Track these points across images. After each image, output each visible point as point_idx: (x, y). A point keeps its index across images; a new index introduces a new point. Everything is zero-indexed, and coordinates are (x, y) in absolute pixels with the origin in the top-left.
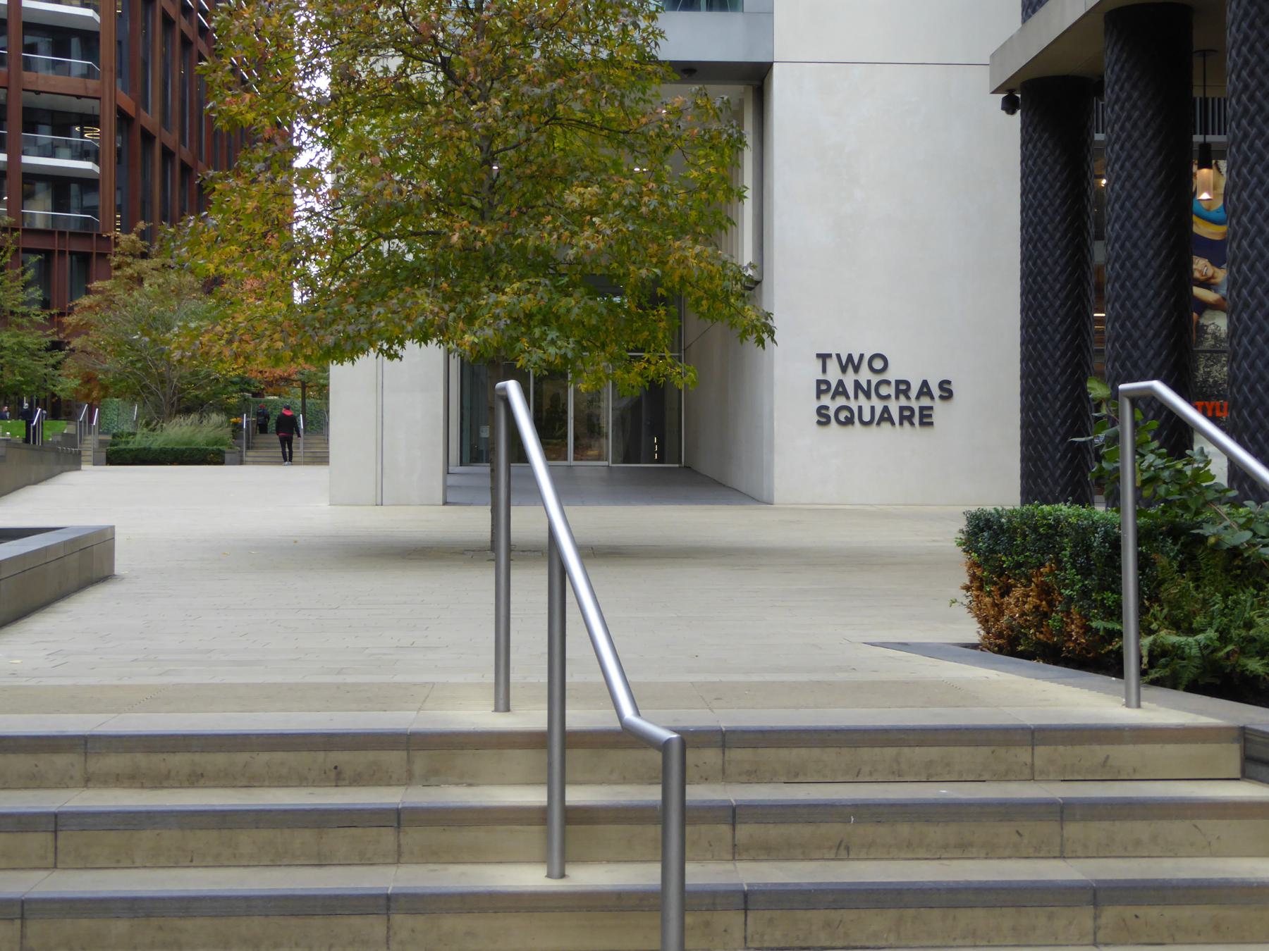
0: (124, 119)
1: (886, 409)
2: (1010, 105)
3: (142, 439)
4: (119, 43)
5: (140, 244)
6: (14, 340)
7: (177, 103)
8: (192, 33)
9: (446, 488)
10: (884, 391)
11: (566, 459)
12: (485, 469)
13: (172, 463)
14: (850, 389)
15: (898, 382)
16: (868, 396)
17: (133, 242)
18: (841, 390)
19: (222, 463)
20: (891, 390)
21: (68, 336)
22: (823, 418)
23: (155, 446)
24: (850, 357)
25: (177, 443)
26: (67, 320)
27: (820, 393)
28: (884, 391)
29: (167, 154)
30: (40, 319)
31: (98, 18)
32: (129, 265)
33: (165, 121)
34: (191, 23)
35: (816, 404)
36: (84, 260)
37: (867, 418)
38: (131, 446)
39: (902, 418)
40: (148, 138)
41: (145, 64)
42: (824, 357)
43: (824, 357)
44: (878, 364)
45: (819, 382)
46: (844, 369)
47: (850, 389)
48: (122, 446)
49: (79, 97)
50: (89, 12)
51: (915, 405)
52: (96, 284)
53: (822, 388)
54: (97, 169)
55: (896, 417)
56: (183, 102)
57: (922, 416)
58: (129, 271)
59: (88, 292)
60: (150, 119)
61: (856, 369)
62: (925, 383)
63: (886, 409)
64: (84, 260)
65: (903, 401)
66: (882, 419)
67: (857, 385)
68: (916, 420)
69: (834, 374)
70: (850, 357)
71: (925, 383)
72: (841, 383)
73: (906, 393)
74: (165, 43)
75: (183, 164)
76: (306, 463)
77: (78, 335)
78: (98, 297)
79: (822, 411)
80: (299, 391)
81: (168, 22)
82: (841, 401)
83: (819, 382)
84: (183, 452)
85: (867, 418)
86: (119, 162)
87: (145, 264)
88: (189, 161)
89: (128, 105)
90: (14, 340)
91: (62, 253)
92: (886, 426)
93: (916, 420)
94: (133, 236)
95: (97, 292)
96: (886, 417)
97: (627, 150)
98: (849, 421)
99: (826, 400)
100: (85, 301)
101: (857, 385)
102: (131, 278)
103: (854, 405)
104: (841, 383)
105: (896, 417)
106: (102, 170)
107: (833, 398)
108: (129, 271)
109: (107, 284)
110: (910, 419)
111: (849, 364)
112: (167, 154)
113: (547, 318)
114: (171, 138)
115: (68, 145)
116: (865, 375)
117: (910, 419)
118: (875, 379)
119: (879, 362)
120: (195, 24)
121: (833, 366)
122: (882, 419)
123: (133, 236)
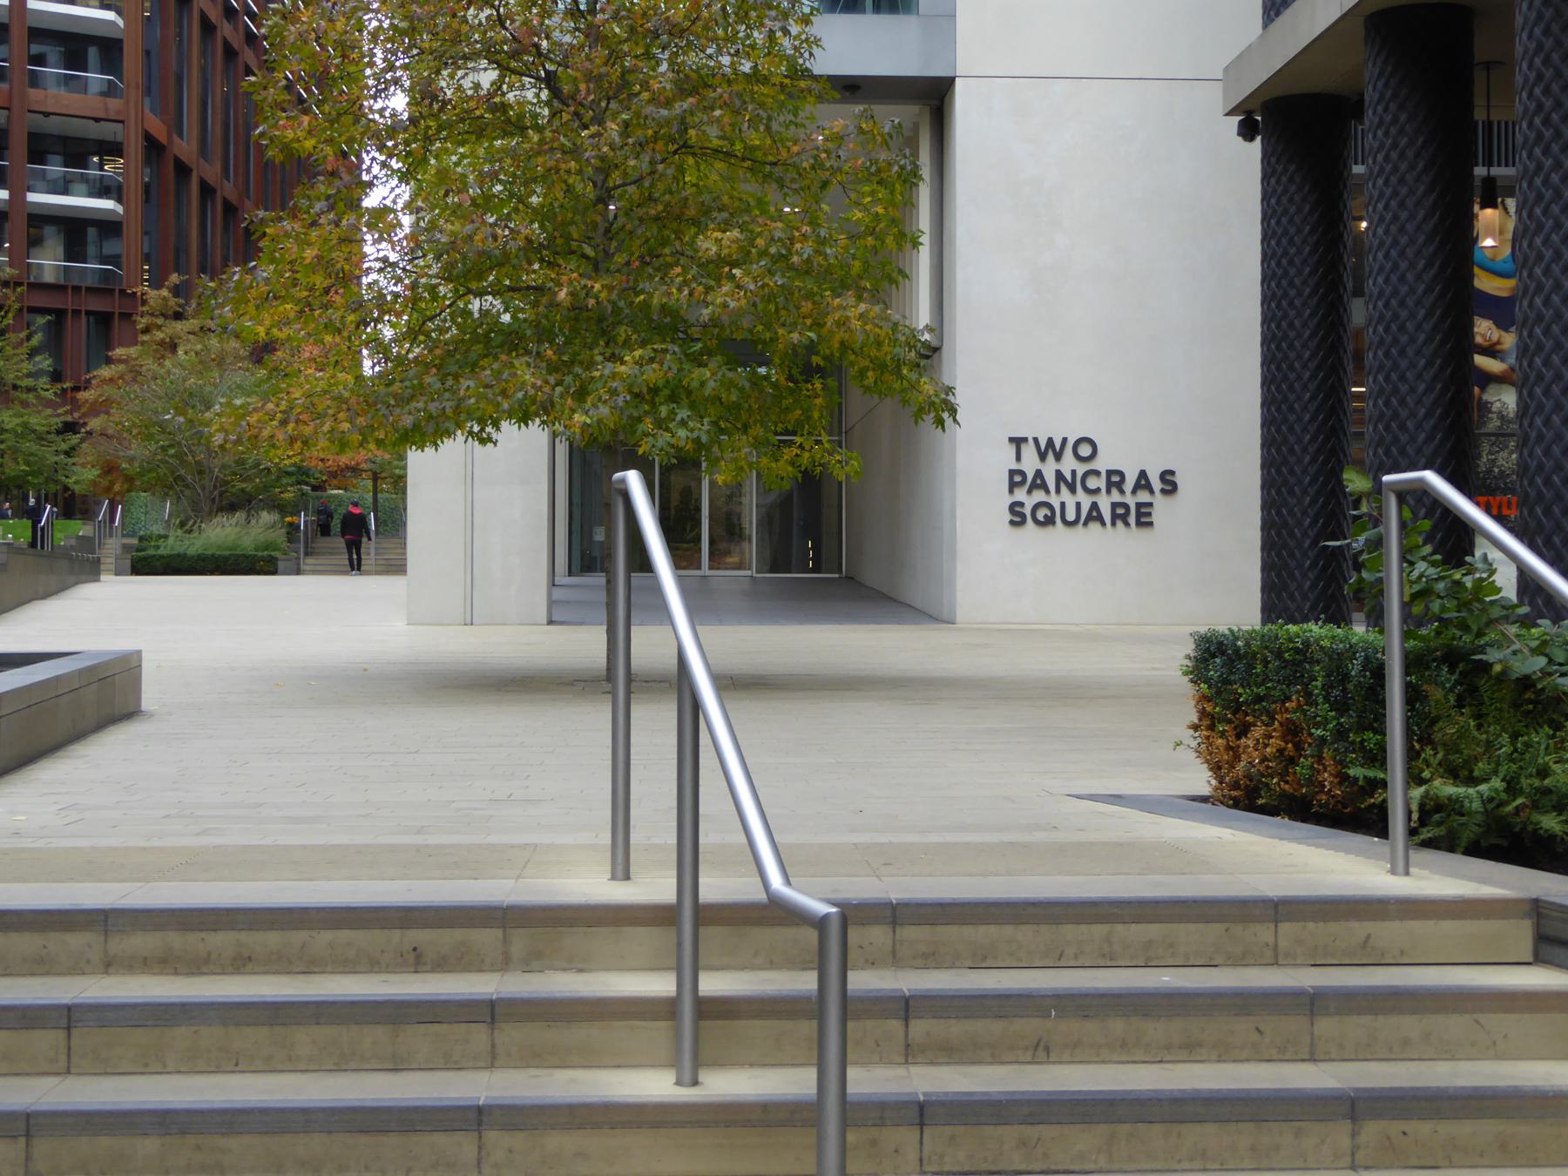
0: (153, 148)
1: (1094, 506)
2: (1248, 130)
3: (176, 543)
4: (148, 53)
5: (172, 302)
6: (17, 421)
7: (218, 128)
8: (237, 41)
9: (551, 603)
10: (1092, 483)
11: (699, 568)
12: (599, 579)
13: (212, 573)
14: (1051, 482)
15: (1110, 473)
16: (1072, 489)
17: (164, 299)
18: (1039, 483)
19: (274, 573)
20: (1101, 483)
21: (84, 415)
22: (1017, 516)
23: (192, 551)
24: (1050, 441)
25: (219, 547)
26: (83, 395)
27: (1013, 486)
28: (1092, 483)
29: (207, 190)
30: (49, 395)
31: (121, 23)
32: (159, 327)
33: (203, 149)
34: (236, 29)
35: (1009, 500)
36: (104, 321)
37: (1071, 516)
38: (161, 552)
39: (1115, 517)
40: (183, 170)
41: (180, 79)
42: (1018, 442)
43: (1018, 442)
44: (1085, 451)
45: (1012, 473)
46: (1043, 457)
47: (1051, 482)
48: (151, 552)
49: (97, 120)
50: (110, 15)
51: (1131, 501)
52: (119, 352)
53: (1016, 479)
54: (120, 209)
55: (1107, 515)
56: (226, 126)
57: (1139, 515)
58: (159, 335)
59: (109, 361)
60: (185, 147)
61: (1058, 457)
62: (1143, 474)
63: (1094, 506)
64: (104, 321)
65: (1116, 496)
66: (1089, 518)
67: (1059, 476)
68: (1132, 519)
69: (1030, 463)
70: (1050, 441)
71: (1143, 474)
72: (1039, 474)
73: (1119, 486)
74: (203, 53)
75: (226, 203)
76: (378, 573)
77: (97, 415)
78: (121, 367)
79: (1015, 508)
80: (370, 483)
81: (208, 27)
82: (1039, 496)
83: (1012, 473)
84: (226, 558)
85: (1071, 516)
86: (147, 201)
87: (179, 326)
88: (233, 199)
89: (158, 129)
90: (17, 421)
91: (76, 313)
92: (1094, 527)
93: (1132, 519)
94: (165, 292)
95: (120, 361)
96: (1095, 515)
97: (774, 185)
98: (1049, 521)
99: (1020, 495)
100: (105, 372)
101: (1059, 476)
102: (162, 343)
103: (1055, 501)
104: (1039, 474)
105: (1107, 515)
106: (126, 210)
107: (1029, 492)
108: (159, 335)
109: (133, 351)
110: (1124, 518)
111: (1049, 450)
112: (207, 190)
113: (676, 393)
114: (211, 171)
115: (84, 179)
116: (1069, 464)
117: (1124, 518)
118: (1081, 469)
119: (1087, 447)
120: (241, 30)
121: (1029, 452)
122: (1089, 518)
123: (165, 292)
